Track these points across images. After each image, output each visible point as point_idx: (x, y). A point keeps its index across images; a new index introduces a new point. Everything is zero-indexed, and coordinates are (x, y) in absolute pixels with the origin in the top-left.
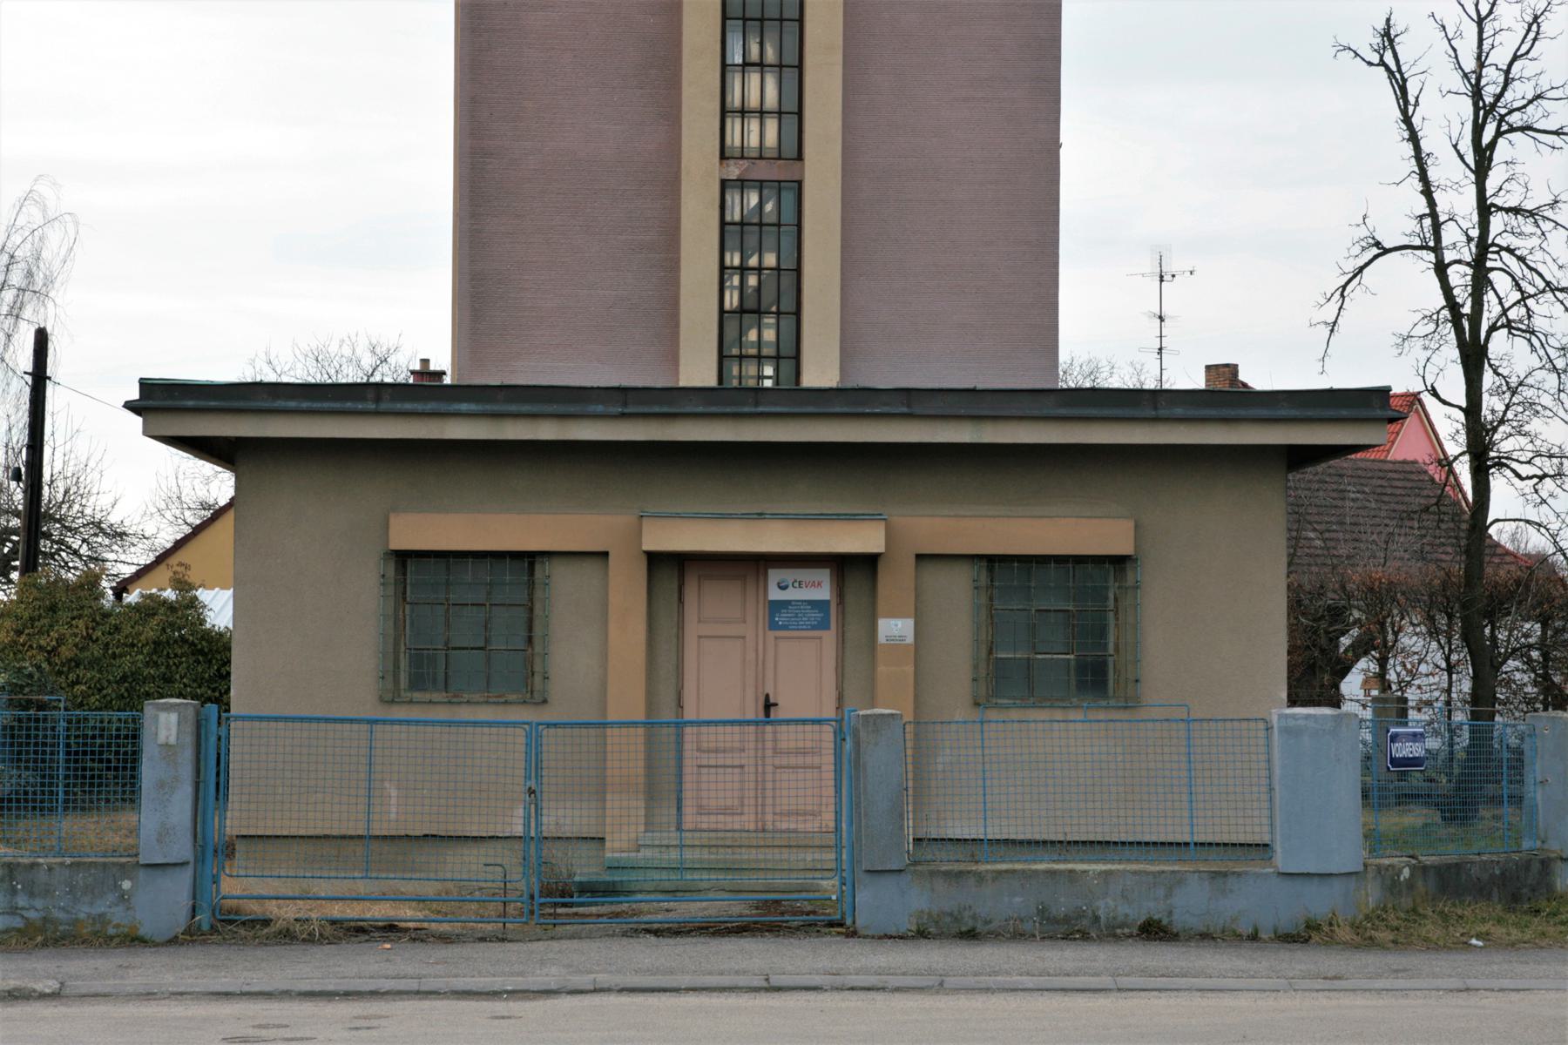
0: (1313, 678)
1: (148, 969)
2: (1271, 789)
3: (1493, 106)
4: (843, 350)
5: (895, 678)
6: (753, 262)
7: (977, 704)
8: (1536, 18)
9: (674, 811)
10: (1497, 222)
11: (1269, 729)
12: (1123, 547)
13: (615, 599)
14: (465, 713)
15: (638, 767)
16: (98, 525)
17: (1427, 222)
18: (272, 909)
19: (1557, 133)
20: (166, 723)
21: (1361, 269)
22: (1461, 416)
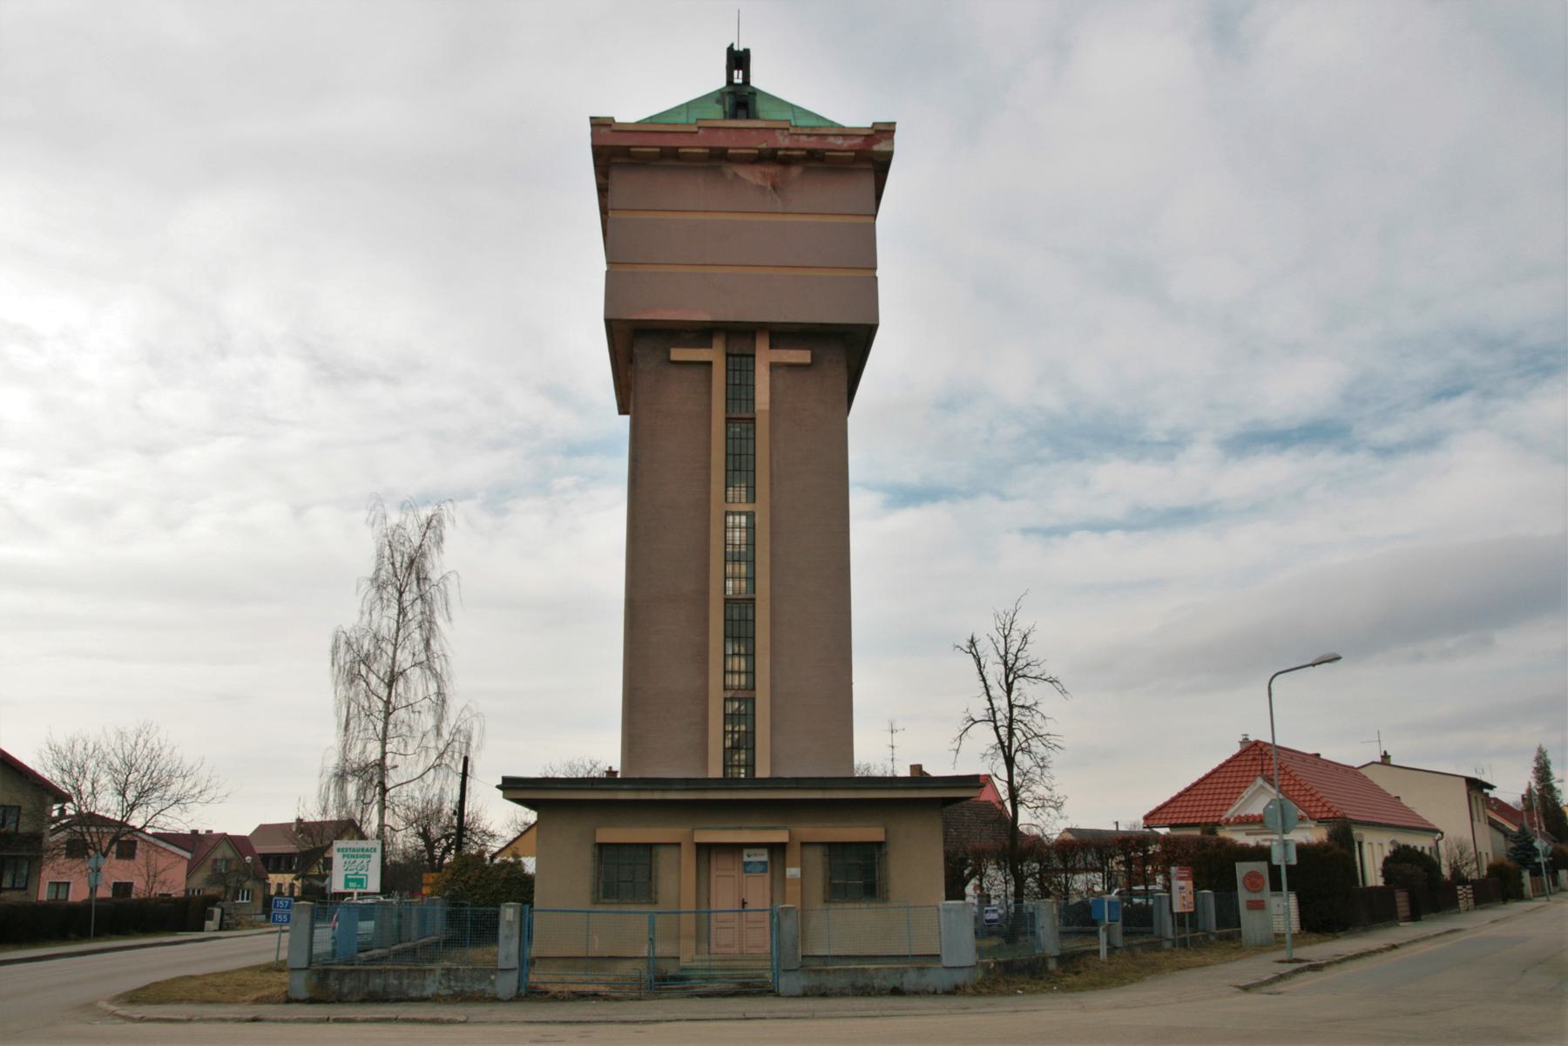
0: (954, 889)
1: (501, 1011)
5: (793, 891)
10: (1016, 711)
12: (881, 838)
13: (683, 861)
14: (625, 908)
15: (693, 929)
18: (549, 987)
20: (509, 913)
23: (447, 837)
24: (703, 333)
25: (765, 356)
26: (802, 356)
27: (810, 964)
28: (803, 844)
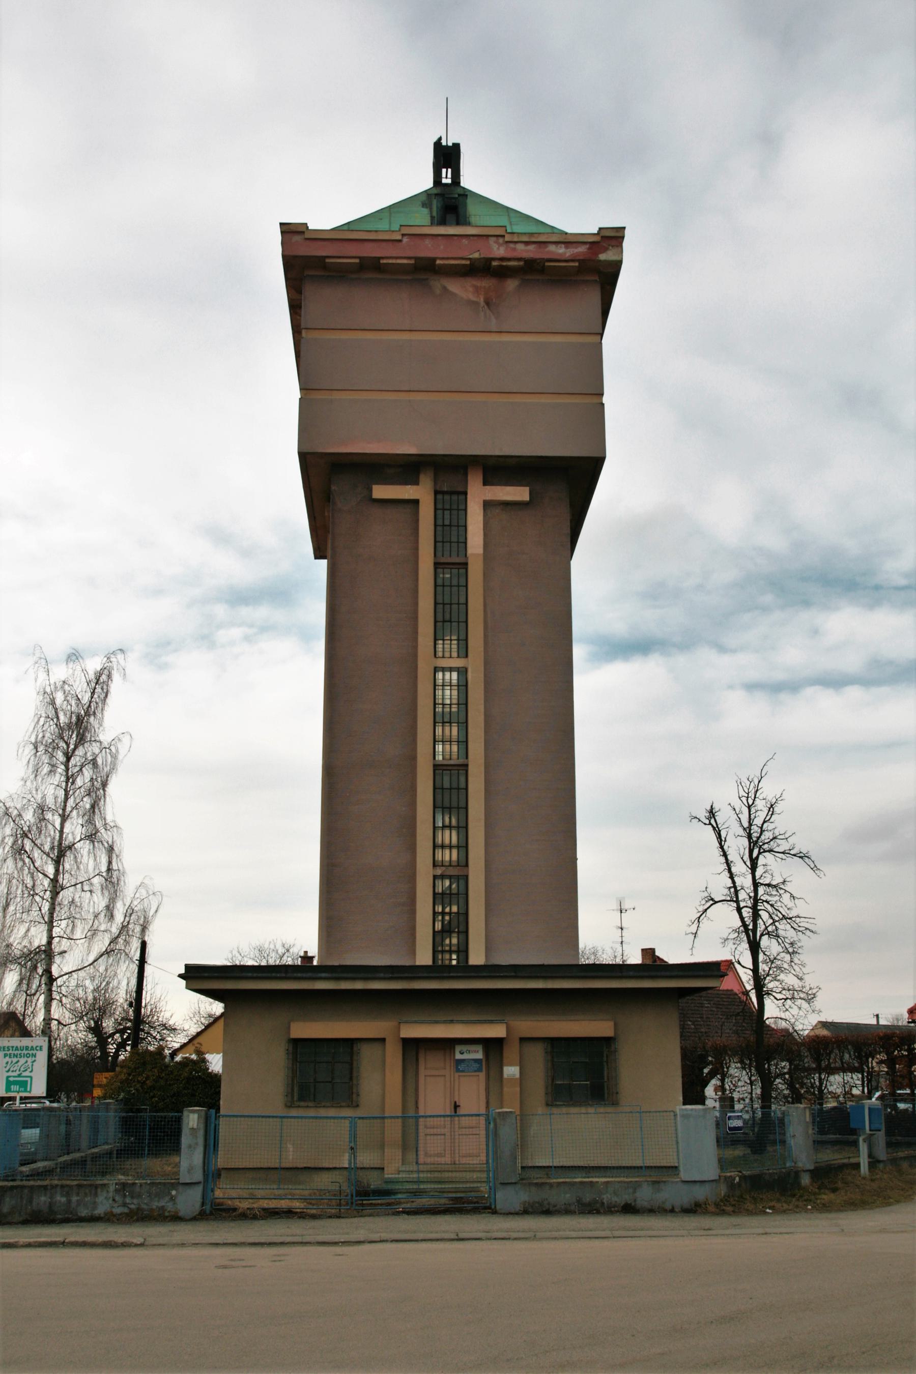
0: (693, 1094)
1: (184, 1232)
2: (677, 1143)
3: (757, 842)
4: (486, 947)
5: (511, 1092)
6: (447, 910)
7: (547, 1105)
8: (772, 806)
9: (415, 1156)
10: (761, 890)
11: (675, 1115)
14: (323, 1112)
16: (164, 1025)
17: (732, 890)
18: (237, 1203)
19: (783, 853)
20: (192, 1119)
21: (706, 910)
22: (751, 973)
23: (122, 1032)
24: (408, 468)
25: (478, 494)
26: (519, 493)
27: (531, 1176)
28: (523, 1040)
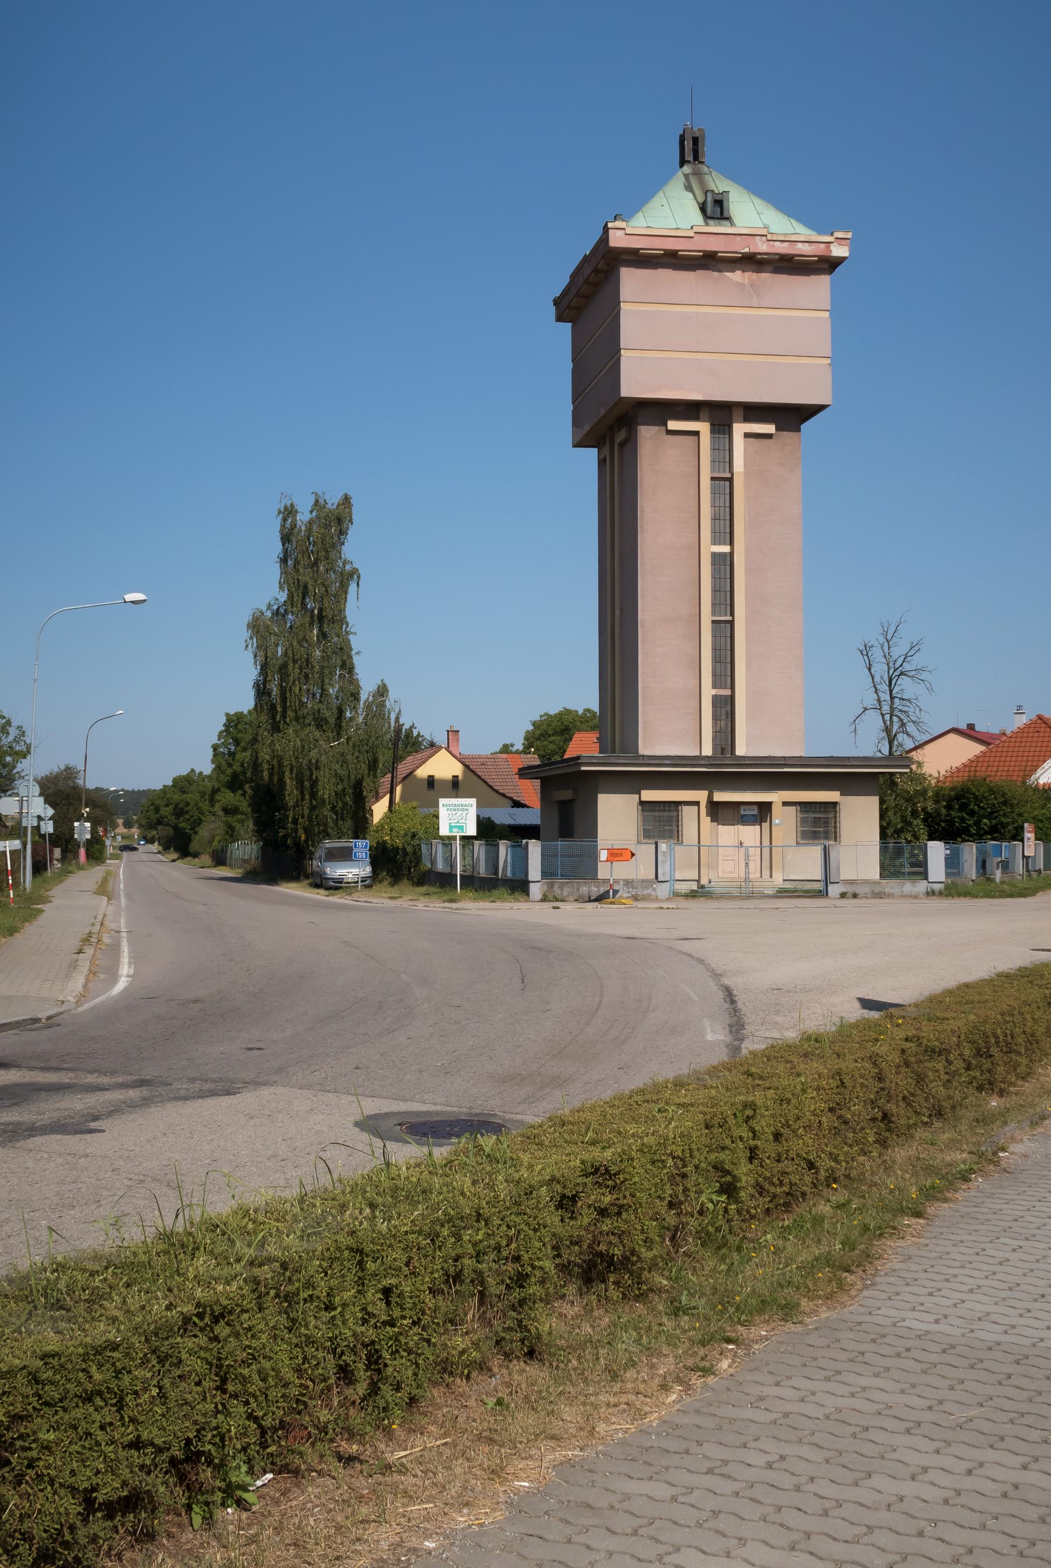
10: (896, 701)
24: (691, 409)
25: (739, 429)
26: (770, 428)
